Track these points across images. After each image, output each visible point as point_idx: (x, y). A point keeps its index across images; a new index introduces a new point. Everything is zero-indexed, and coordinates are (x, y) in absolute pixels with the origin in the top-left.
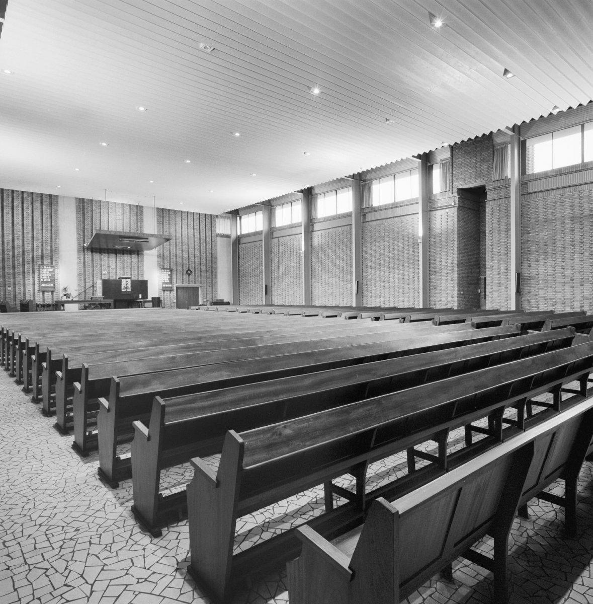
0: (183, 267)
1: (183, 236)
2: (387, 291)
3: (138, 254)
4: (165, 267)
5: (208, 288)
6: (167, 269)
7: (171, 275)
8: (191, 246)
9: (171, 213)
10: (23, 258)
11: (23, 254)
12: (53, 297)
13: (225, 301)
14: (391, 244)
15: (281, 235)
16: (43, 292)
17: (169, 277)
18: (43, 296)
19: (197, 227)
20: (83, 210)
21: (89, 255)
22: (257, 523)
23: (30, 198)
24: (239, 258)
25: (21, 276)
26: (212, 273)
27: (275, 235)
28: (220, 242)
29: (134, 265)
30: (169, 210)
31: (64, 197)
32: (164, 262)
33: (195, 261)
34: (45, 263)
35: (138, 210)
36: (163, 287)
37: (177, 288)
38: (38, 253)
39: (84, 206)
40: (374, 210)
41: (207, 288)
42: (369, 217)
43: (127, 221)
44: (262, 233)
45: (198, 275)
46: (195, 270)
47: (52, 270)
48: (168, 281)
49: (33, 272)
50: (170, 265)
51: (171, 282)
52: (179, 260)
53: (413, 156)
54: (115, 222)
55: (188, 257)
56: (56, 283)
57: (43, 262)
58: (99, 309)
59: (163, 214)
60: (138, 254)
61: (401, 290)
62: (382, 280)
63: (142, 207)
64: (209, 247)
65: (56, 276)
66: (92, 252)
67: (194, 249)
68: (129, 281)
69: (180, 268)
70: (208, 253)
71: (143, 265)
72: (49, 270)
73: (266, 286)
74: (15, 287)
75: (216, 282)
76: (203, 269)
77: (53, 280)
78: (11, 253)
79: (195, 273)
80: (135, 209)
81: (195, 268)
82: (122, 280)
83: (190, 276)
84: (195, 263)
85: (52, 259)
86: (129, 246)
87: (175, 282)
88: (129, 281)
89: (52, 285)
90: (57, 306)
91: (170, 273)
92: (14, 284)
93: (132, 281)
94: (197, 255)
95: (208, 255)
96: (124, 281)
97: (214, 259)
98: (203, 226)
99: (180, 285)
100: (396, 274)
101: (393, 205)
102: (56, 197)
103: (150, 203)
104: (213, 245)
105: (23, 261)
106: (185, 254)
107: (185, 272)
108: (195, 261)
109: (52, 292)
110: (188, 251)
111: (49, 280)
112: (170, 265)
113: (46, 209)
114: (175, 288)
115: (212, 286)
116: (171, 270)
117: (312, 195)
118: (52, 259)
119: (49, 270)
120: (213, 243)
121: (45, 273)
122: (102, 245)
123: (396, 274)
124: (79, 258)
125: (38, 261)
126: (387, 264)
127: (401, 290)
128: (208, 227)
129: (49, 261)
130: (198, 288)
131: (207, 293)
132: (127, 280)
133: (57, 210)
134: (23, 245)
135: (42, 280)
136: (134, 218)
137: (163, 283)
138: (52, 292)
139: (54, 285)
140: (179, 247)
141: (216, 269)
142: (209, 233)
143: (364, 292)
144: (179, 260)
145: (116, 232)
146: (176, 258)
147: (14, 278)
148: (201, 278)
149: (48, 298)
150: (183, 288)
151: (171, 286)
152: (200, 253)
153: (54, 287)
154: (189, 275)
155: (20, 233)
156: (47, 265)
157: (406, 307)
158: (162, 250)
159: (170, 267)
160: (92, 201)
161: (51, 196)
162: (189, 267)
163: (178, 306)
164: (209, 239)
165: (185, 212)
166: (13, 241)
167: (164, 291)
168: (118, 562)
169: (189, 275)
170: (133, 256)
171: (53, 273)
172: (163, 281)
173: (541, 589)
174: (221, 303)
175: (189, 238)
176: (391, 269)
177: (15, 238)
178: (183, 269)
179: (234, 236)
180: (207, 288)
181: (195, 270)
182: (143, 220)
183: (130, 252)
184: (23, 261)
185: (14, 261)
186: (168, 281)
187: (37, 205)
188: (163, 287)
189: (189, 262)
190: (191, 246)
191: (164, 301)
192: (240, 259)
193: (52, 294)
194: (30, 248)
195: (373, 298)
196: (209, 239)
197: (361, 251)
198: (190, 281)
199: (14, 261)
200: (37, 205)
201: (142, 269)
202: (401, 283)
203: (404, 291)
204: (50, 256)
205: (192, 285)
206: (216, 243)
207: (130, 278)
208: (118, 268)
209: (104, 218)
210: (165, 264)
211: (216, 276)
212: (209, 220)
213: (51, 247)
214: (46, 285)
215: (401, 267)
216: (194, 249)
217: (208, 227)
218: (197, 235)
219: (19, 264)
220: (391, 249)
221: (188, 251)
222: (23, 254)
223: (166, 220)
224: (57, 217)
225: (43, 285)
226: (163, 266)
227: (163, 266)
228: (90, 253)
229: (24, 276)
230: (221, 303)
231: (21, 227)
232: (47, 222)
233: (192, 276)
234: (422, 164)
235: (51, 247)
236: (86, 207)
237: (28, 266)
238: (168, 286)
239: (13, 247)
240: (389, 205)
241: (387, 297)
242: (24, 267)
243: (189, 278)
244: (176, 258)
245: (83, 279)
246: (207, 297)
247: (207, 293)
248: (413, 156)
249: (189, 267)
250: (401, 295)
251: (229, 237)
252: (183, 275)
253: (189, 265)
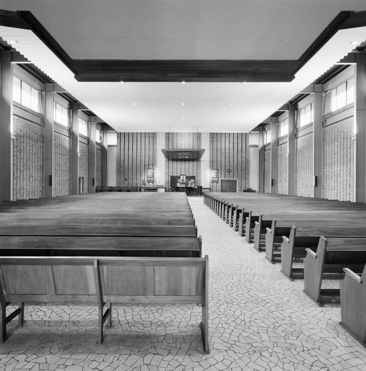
0: (225, 168)
1: (226, 149)
2: (339, 184)
3: (198, 161)
4: (214, 168)
5: (243, 180)
6: (215, 169)
7: (217, 173)
8: (231, 154)
9: (218, 135)
10: (141, 166)
11: (141, 164)
12: (149, 185)
13: (253, 189)
14: (342, 143)
15: (283, 143)
16: (149, 182)
17: (216, 174)
18: (149, 184)
19: (236, 142)
20: (169, 139)
21: (171, 162)
22: (200, 313)
23: (144, 136)
24: (264, 160)
25: (139, 174)
26: (246, 171)
27: (280, 143)
28: (251, 149)
29: (195, 167)
30: (217, 133)
31: (159, 133)
32: (213, 165)
33: (233, 163)
34: (150, 168)
35: (198, 136)
36: (212, 180)
37: (222, 181)
38: (147, 163)
39: (169, 136)
40: (331, 115)
41: (241, 181)
42: (329, 122)
43: (191, 142)
44: (270, 144)
45: (235, 172)
46: (233, 170)
47: (153, 171)
48: (216, 177)
49: (145, 172)
50: (217, 166)
51: (217, 177)
52: (223, 164)
53: (338, 62)
54: (184, 144)
55: (229, 161)
56: (155, 178)
57: (149, 167)
58: (175, 192)
59: (213, 136)
60: (198, 161)
61: (348, 185)
62: (336, 175)
63: (201, 133)
64: (244, 154)
65: (155, 174)
66: (173, 161)
67: (233, 156)
68: (185, 176)
69: (223, 168)
70: (243, 158)
71: (200, 167)
72: (151, 171)
73: (272, 180)
74: (136, 180)
75: (249, 177)
76: (240, 168)
77: (153, 176)
78: (135, 163)
79: (233, 172)
80: (196, 135)
81: (233, 168)
82: (181, 176)
83: (230, 173)
84: (233, 165)
85: (153, 165)
86: (194, 156)
87: (220, 177)
88: (185, 176)
89: (153, 179)
90: (155, 190)
91: (216, 171)
92: (136, 178)
93: (186, 176)
94: (235, 160)
95: (243, 159)
96: (182, 177)
97: (247, 162)
98: (240, 141)
99: (223, 179)
100: (345, 170)
101: (343, 109)
102: (156, 133)
103: (206, 130)
104: (247, 153)
105: (141, 167)
106: (227, 160)
107: (226, 171)
108: (233, 163)
109: (153, 182)
110: (229, 157)
111: (151, 176)
112: (217, 166)
113: (151, 140)
114: (220, 181)
115: (245, 180)
116: (217, 170)
117: (297, 110)
118: (153, 165)
119: (151, 171)
120: (247, 151)
121: (150, 172)
122: (173, 156)
123: (345, 170)
124: (166, 164)
125: (147, 167)
126: (336, 163)
127: (348, 185)
128: (244, 141)
129: (152, 166)
130: (236, 181)
131: (241, 184)
132: (183, 176)
133: (156, 140)
134: (141, 159)
135: (148, 176)
136: (196, 140)
137: (212, 178)
138: (153, 182)
139: (154, 179)
140: (223, 155)
141: (249, 168)
142: (244, 145)
143: (325, 185)
144: (223, 164)
145: (185, 149)
146: (221, 163)
147: (136, 175)
148: (237, 175)
149: (151, 185)
150: (226, 181)
151: (217, 179)
152: (237, 158)
153: (153, 180)
154: (229, 173)
155: (140, 153)
156: (151, 169)
157: (333, 199)
158: (212, 158)
159: (217, 168)
160: (173, 133)
161: (153, 133)
162: (229, 168)
163: (222, 192)
164: (244, 149)
165: (227, 133)
166: (137, 157)
167: (213, 183)
168: (269, 336)
169: (229, 173)
170: (178, 162)
171: (153, 173)
172: (212, 177)
173: (105, 355)
174: (249, 191)
175: (230, 149)
176: (342, 164)
177: (138, 156)
178: (225, 169)
179: (261, 145)
180: (241, 181)
181: (233, 170)
182: (201, 141)
183: (193, 160)
184: (141, 167)
185: (136, 167)
186: (216, 177)
187: (147, 139)
188: (212, 180)
189: (229, 164)
190: (231, 154)
191: (213, 189)
192: (265, 161)
193: (153, 183)
194: (144, 160)
195: (330, 190)
196: (244, 149)
197: (322, 151)
198: (230, 176)
199: (136, 167)
200: (147, 139)
201: (200, 169)
202: (348, 178)
203: (350, 185)
204: (152, 164)
205: (231, 179)
206: (249, 151)
207: (185, 175)
208: (183, 169)
209: (179, 142)
210: (213, 165)
211: (249, 173)
212: (244, 137)
213: (153, 159)
214: (150, 179)
215: (348, 163)
216: (233, 156)
217: (244, 141)
218: (236, 147)
219: (138, 169)
220: (342, 148)
221: (229, 157)
222: (141, 164)
223: (215, 140)
224: (156, 144)
225: (149, 179)
226: (213, 167)
227: (213, 167)
228: (171, 162)
229: (141, 174)
230: (249, 191)
231: (140, 150)
232: (151, 146)
233: (231, 173)
234: (357, 67)
235: (153, 159)
236: (170, 137)
237: (143, 169)
238: (215, 179)
239: (137, 160)
240: (341, 109)
241: (339, 190)
242: (140, 170)
243: (229, 174)
244: (221, 163)
245: (167, 176)
246: (241, 187)
247: (241, 184)
248: (338, 62)
249: (229, 168)
250: (348, 189)
251: (257, 146)
252: (225, 172)
253: (229, 166)
